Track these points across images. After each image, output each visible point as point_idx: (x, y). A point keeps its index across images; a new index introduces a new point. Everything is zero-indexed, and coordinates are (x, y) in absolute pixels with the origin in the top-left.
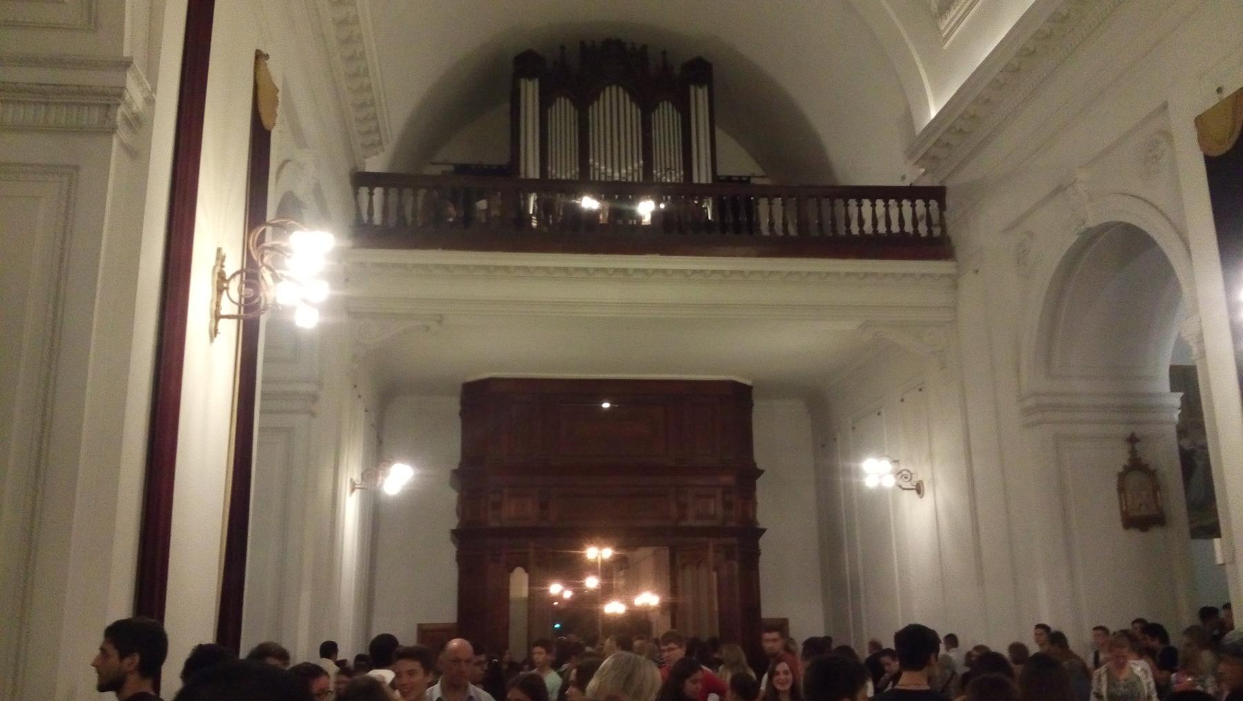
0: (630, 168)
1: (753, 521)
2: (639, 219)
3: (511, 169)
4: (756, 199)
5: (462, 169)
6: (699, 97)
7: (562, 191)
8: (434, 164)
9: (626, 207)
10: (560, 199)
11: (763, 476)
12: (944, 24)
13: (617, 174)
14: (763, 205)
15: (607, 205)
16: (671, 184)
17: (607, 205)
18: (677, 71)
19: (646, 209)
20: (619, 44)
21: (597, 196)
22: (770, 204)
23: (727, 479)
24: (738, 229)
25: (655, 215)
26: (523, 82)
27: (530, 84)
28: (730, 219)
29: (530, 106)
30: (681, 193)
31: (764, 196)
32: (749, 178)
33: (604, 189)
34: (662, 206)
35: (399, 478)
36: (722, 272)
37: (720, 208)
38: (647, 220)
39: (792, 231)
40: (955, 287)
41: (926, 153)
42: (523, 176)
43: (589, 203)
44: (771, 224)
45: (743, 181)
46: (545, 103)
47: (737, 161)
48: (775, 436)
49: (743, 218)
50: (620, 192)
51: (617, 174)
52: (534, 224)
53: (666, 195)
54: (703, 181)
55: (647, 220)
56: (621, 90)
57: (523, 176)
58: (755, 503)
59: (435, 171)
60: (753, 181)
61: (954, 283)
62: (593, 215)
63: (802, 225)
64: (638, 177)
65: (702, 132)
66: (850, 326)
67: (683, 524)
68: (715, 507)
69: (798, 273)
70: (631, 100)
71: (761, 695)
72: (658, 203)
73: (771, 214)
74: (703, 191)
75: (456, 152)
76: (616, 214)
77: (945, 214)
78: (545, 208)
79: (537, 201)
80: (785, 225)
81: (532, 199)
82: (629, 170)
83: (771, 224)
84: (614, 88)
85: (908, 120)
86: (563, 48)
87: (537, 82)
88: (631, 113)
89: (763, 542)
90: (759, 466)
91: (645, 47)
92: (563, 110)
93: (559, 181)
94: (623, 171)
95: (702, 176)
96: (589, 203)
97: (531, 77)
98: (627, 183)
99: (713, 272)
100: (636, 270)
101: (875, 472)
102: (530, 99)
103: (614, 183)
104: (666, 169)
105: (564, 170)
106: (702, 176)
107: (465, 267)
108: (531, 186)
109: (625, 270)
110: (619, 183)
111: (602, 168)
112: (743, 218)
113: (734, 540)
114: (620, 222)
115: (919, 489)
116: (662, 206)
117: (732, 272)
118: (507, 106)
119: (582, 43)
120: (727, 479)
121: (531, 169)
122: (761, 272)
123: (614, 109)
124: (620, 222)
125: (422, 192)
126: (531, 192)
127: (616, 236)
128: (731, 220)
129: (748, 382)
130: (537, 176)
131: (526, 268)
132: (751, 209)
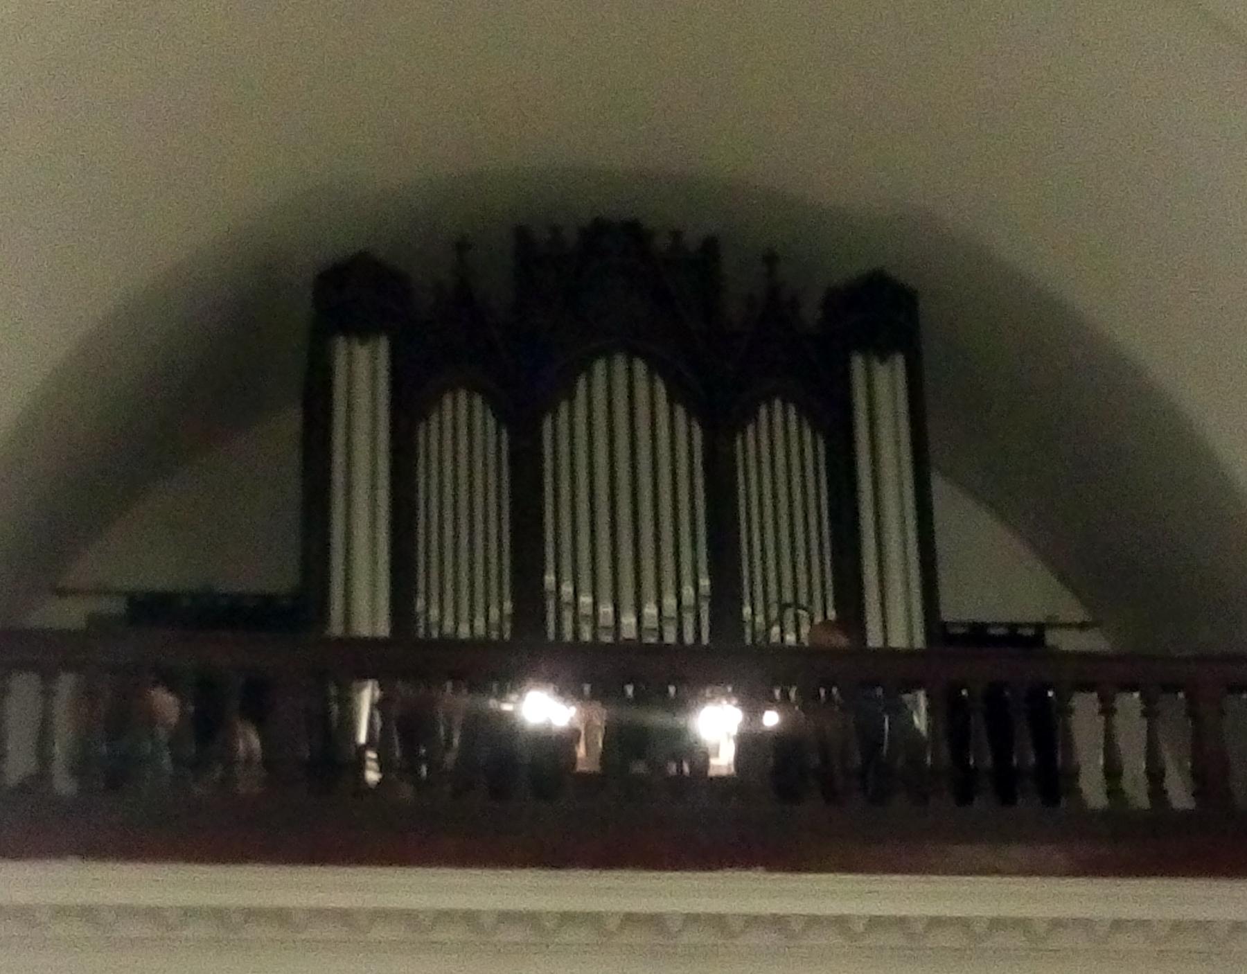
0: (670, 602)
2: (700, 757)
3: (300, 609)
4: (1064, 697)
5: (149, 609)
6: (880, 388)
7: (458, 676)
8: (61, 593)
9: (657, 719)
10: (454, 702)
13: (629, 620)
14: (1085, 706)
15: (600, 715)
16: (798, 650)
17: (600, 715)
19: (718, 727)
20: (633, 233)
21: (568, 690)
22: (1108, 711)
24: (1006, 787)
25: (749, 744)
26: (341, 347)
27: (362, 353)
28: (982, 758)
29: (362, 422)
30: (832, 676)
31: (1087, 687)
32: (1040, 628)
33: (598, 669)
34: (771, 719)
36: (964, 924)
37: (950, 710)
38: (723, 760)
39: (1180, 795)
42: (336, 629)
43: (542, 709)
44: (1112, 772)
45: (1025, 640)
46: (408, 408)
47: (1002, 579)
49: (1026, 756)
50: (641, 678)
51: (629, 620)
52: (372, 776)
53: (786, 683)
54: (898, 640)
55: (723, 760)
56: (640, 367)
57: (336, 629)
59: (68, 614)
60: (1052, 638)
62: (556, 747)
63: (1209, 777)
64: (696, 630)
65: (888, 473)
66: (335, 725)
69: (1203, 926)
70: (671, 400)
72: (753, 709)
73: (1108, 743)
74: (900, 671)
75: (144, 555)
76: (625, 743)
78: (406, 728)
79: (379, 706)
80: (1155, 775)
81: (366, 697)
82: (668, 608)
83: (1112, 772)
84: (620, 364)
86: (462, 246)
87: (383, 347)
88: (674, 437)
91: (711, 246)
92: (464, 431)
93: (450, 644)
94: (650, 610)
95: (895, 624)
96: (542, 709)
97: (361, 330)
98: (661, 648)
99: (936, 923)
102: (363, 402)
103: (621, 649)
104: (783, 607)
105: (464, 608)
106: (895, 624)
107: (153, 914)
108: (363, 658)
109: (655, 921)
110: (637, 648)
111: (587, 605)
112: (1026, 756)
114: (639, 768)
116: (771, 719)
117: (996, 924)
118: (291, 421)
121: (365, 609)
122: (1086, 924)
123: (620, 424)
124: (639, 768)
125: (66, 683)
126: (364, 676)
127: (632, 812)
128: (988, 761)
130: (383, 629)
131: (344, 916)
132: (1049, 729)
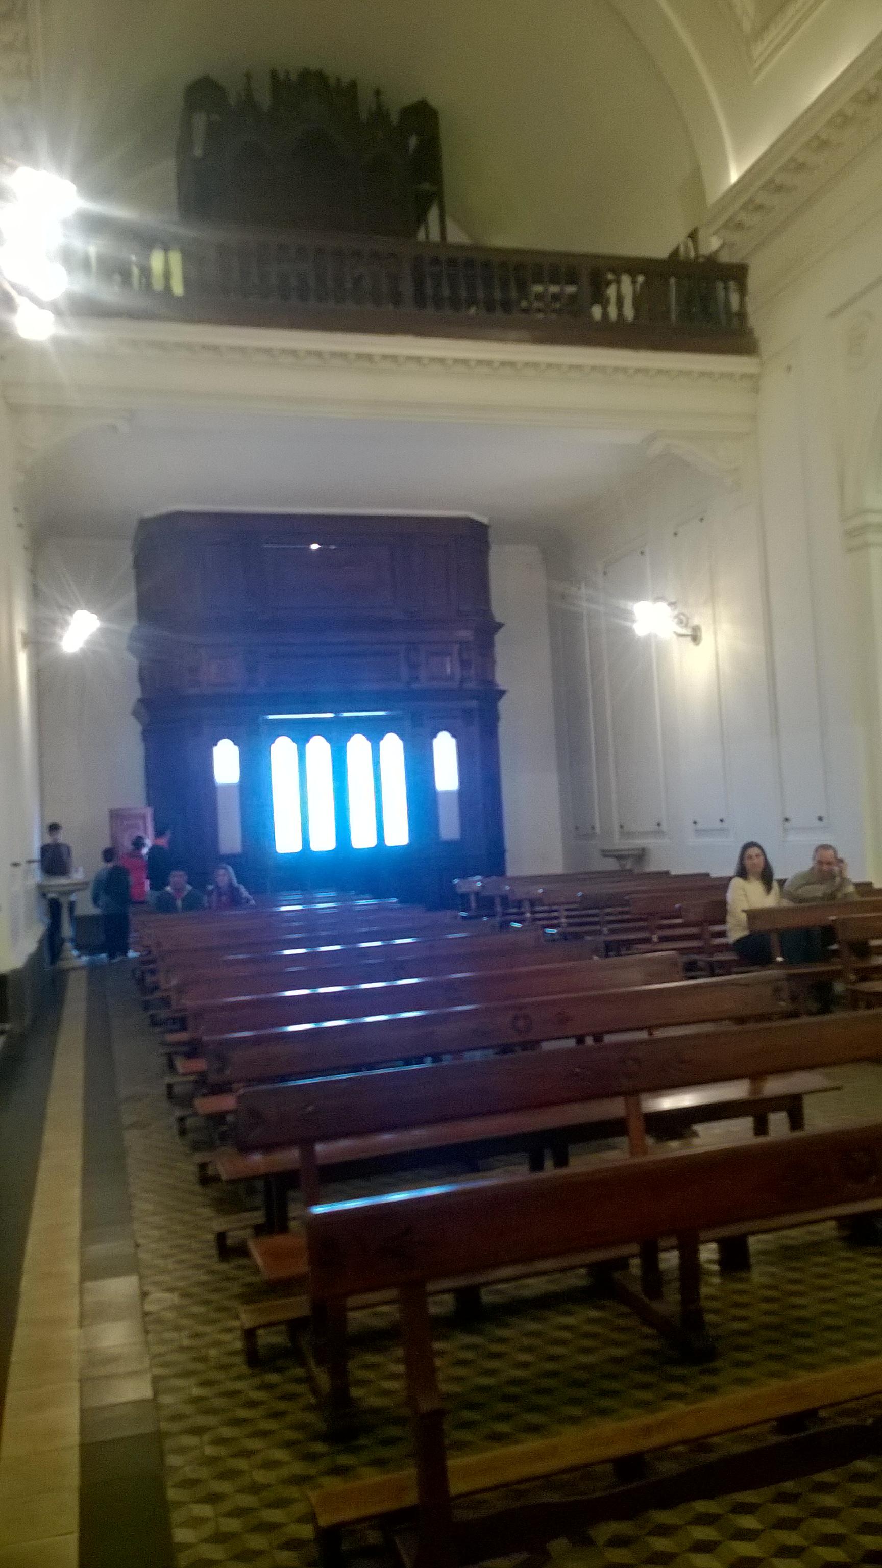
1: (491, 683)
11: (502, 630)
12: (758, 49)
18: (395, 119)
20: (320, 76)
23: (465, 634)
35: (81, 630)
40: (756, 390)
41: (731, 219)
48: (512, 580)
58: (493, 662)
61: (754, 383)
67: (415, 686)
68: (449, 667)
71: (277, 953)
77: (747, 298)
85: (695, 183)
89: (503, 705)
90: (498, 617)
91: (353, 85)
100: (385, 357)
101: (649, 618)
113: (474, 704)
115: (695, 638)
119: (274, 74)
120: (465, 634)
129: (484, 520)
